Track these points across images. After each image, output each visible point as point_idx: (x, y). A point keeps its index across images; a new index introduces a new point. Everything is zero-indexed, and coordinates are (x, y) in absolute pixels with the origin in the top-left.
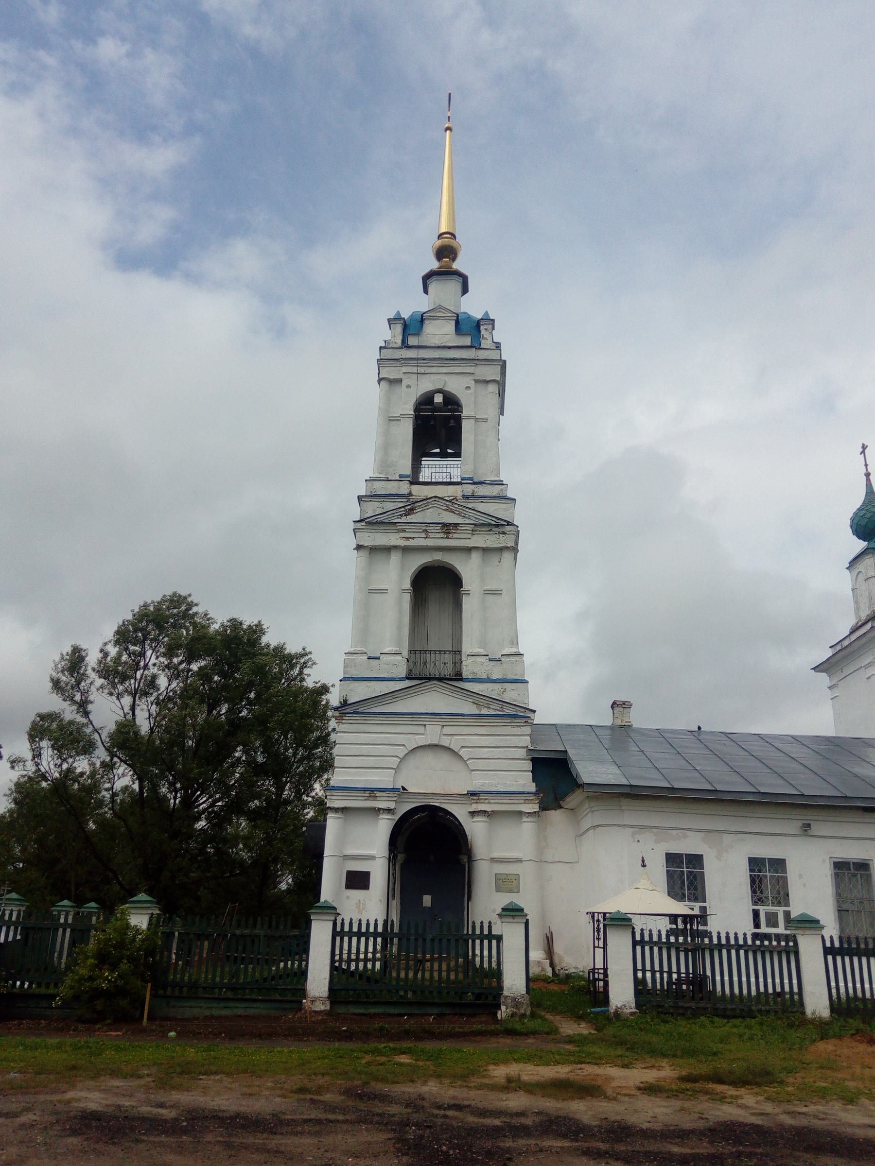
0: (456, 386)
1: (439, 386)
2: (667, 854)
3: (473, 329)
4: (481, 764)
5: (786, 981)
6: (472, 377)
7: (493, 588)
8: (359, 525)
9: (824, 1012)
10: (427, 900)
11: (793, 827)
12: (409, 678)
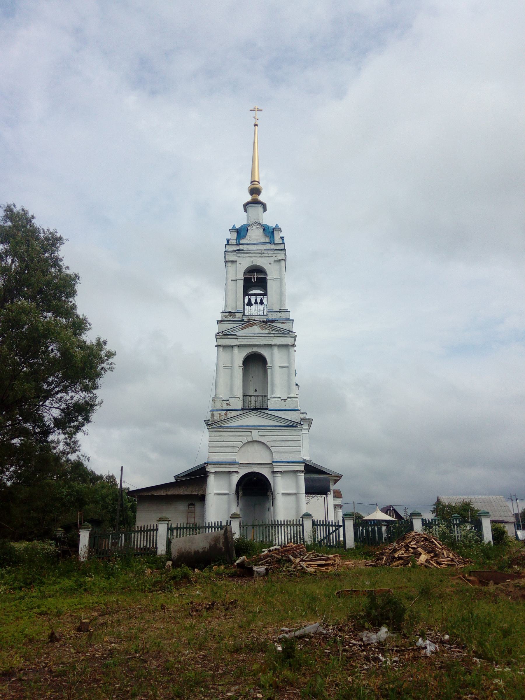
3: (270, 232)
12: (242, 410)
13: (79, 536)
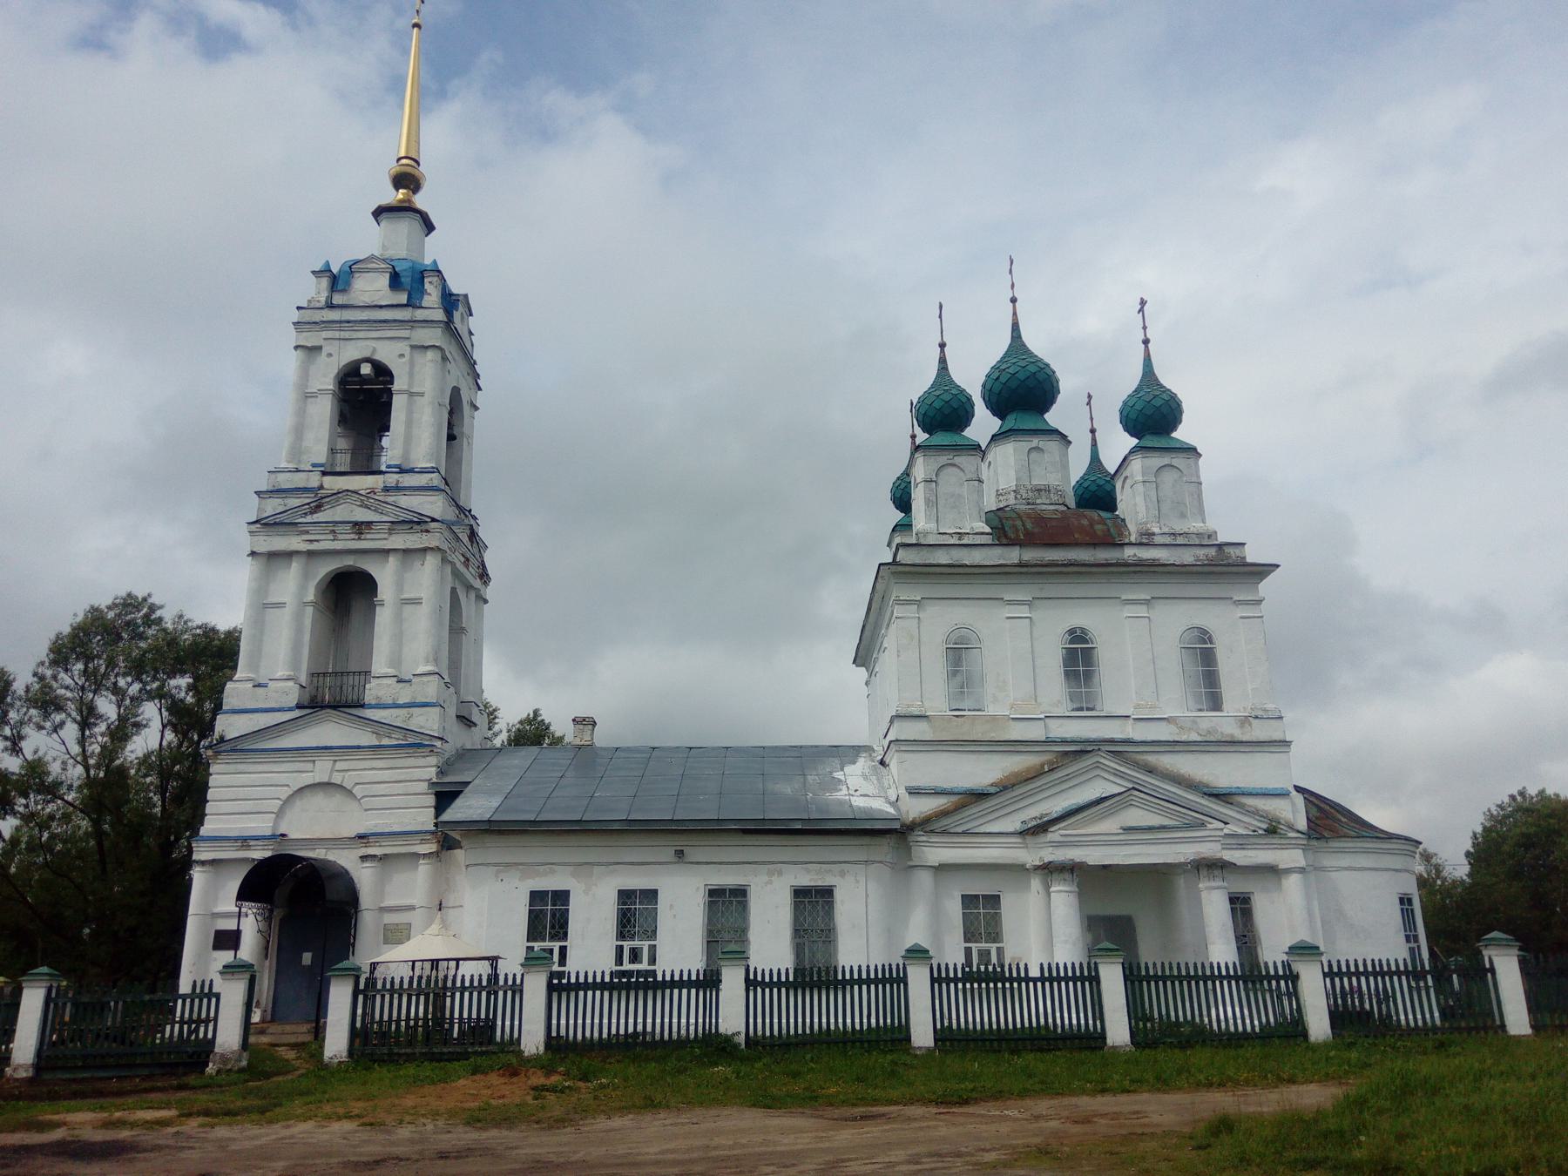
0: (388, 353)
1: (367, 354)
2: (532, 893)
4: (378, 802)
5: (649, 1020)
6: (406, 343)
7: (412, 596)
8: (253, 528)
9: (930, 1043)
10: (307, 958)
11: (668, 854)
12: (299, 707)
13: (1333, 1027)
